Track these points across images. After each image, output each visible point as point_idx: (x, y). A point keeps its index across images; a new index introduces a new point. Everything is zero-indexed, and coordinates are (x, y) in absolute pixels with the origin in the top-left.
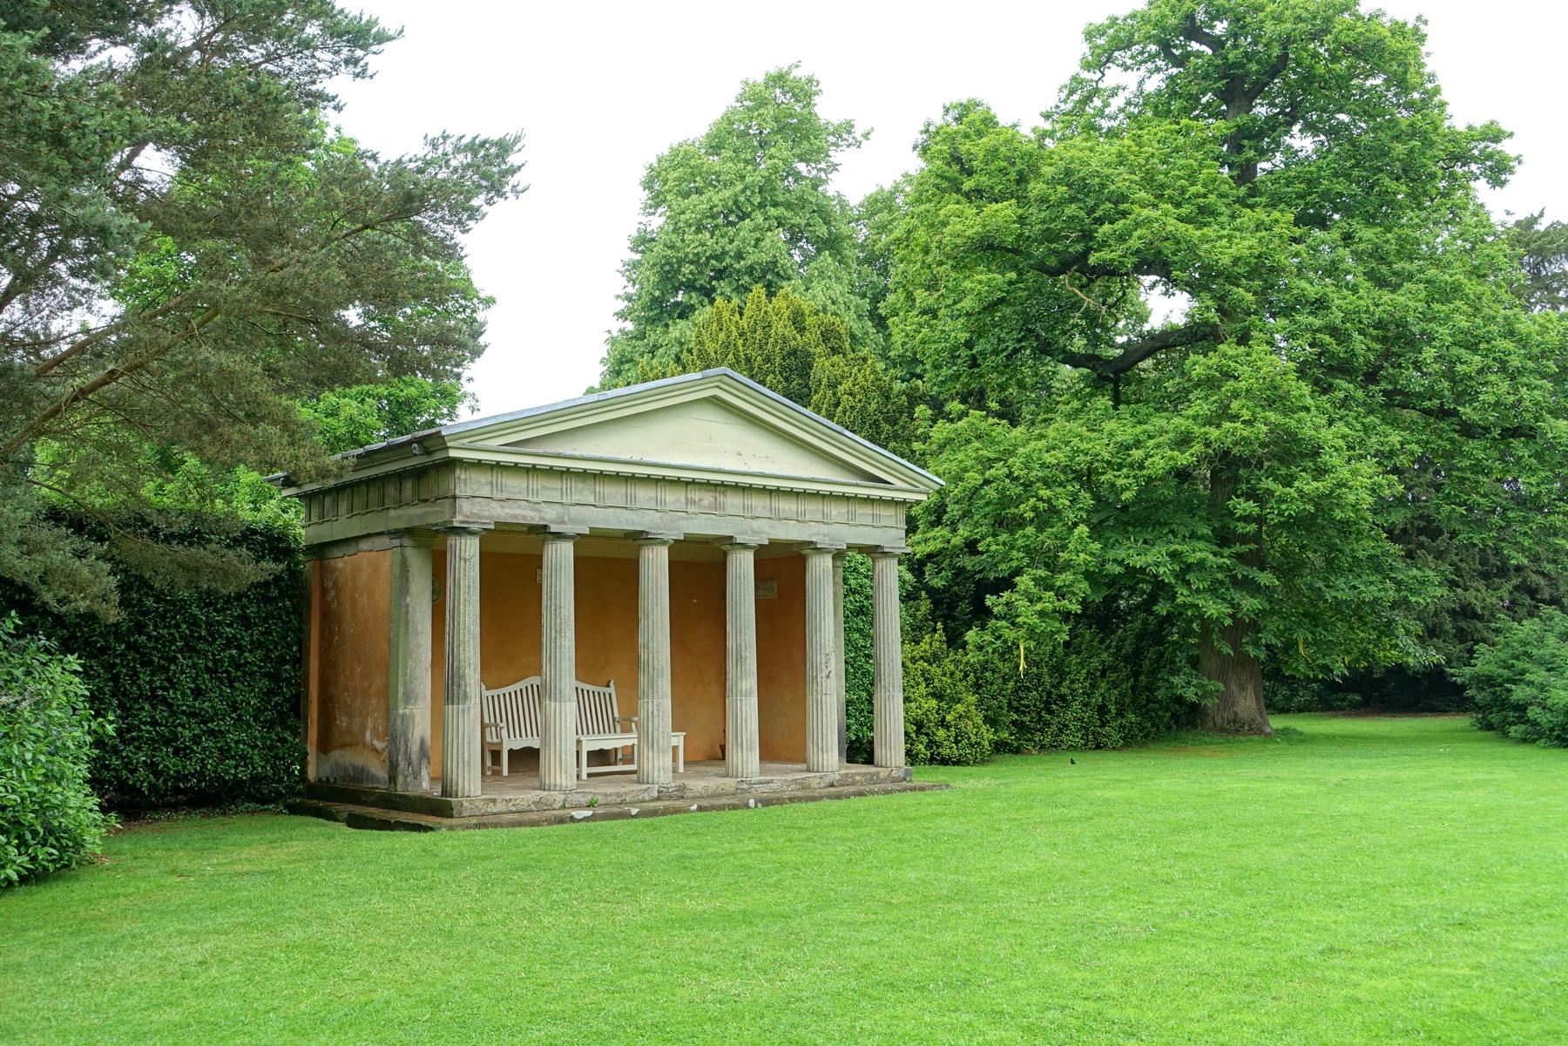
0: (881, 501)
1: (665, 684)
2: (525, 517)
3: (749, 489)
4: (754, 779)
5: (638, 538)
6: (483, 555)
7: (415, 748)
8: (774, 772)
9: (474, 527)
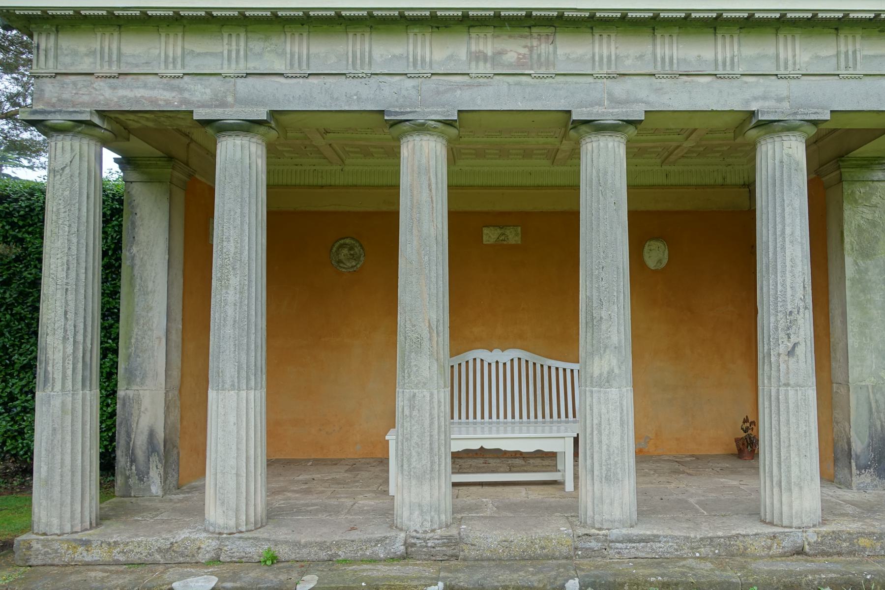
4: (615, 533)
7: (140, 440)
8: (680, 508)
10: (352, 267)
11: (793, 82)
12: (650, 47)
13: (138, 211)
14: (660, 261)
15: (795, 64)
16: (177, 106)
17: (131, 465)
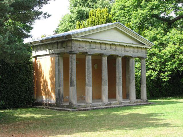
2: (84, 51)
5: (102, 55)
6: (92, 60)
9: (76, 53)
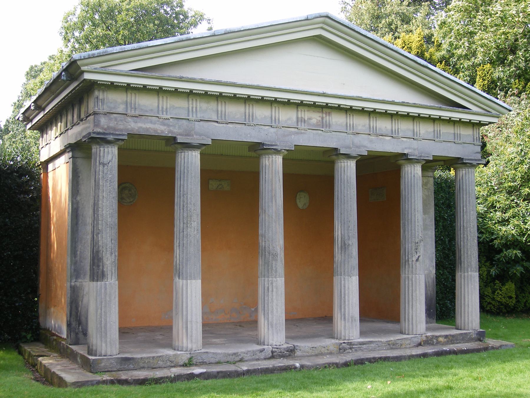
0: (460, 122)
1: (196, 223)
2: (155, 131)
3: (350, 110)
5: (258, 149)
6: (123, 169)
9: (111, 138)
10: (130, 202)
11: (419, 142)
12: (368, 121)
13: (80, 175)
14: (305, 204)
15: (420, 134)
16: (167, 134)
17: (79, 326)
